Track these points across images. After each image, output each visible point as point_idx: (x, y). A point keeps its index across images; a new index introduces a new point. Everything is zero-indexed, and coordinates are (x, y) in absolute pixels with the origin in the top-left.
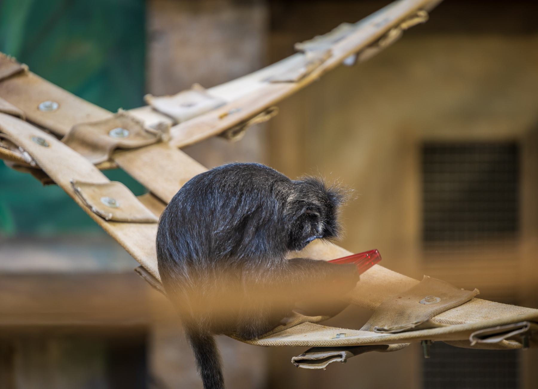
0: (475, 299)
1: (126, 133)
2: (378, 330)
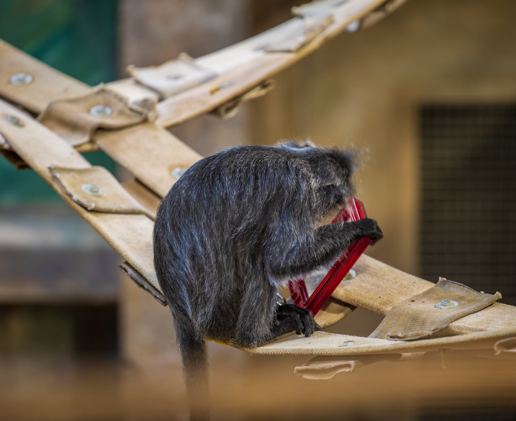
0: (496, 303)
1: (108, 111)
2: (392, 337)
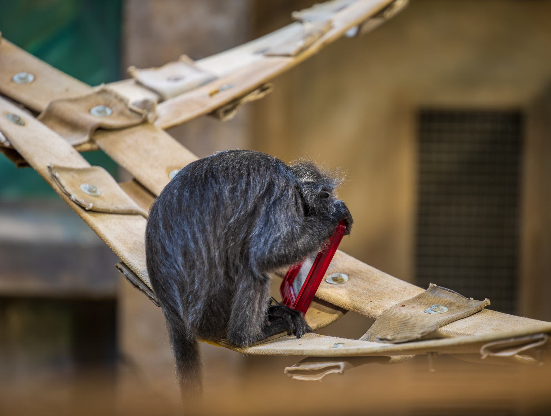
0: (485, 309)
1: (109, 111)
